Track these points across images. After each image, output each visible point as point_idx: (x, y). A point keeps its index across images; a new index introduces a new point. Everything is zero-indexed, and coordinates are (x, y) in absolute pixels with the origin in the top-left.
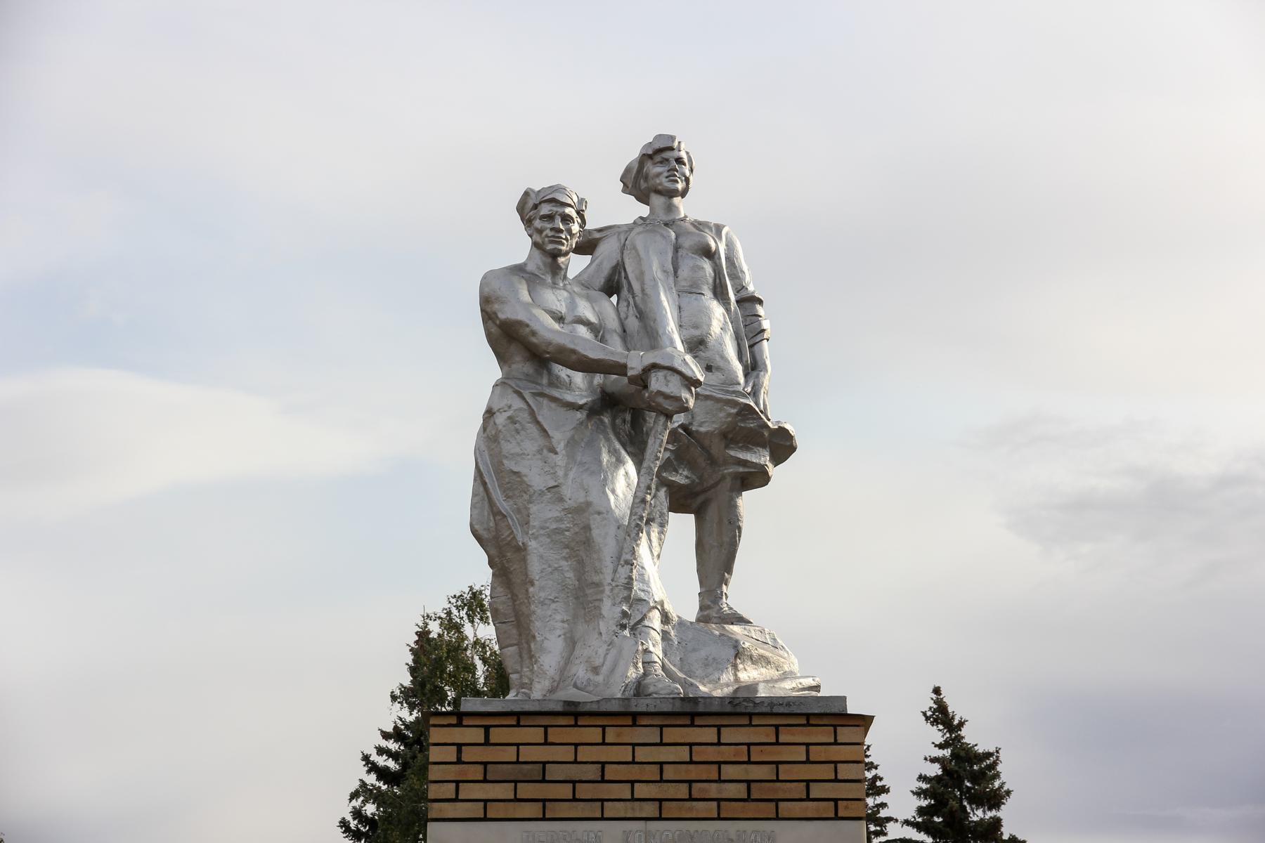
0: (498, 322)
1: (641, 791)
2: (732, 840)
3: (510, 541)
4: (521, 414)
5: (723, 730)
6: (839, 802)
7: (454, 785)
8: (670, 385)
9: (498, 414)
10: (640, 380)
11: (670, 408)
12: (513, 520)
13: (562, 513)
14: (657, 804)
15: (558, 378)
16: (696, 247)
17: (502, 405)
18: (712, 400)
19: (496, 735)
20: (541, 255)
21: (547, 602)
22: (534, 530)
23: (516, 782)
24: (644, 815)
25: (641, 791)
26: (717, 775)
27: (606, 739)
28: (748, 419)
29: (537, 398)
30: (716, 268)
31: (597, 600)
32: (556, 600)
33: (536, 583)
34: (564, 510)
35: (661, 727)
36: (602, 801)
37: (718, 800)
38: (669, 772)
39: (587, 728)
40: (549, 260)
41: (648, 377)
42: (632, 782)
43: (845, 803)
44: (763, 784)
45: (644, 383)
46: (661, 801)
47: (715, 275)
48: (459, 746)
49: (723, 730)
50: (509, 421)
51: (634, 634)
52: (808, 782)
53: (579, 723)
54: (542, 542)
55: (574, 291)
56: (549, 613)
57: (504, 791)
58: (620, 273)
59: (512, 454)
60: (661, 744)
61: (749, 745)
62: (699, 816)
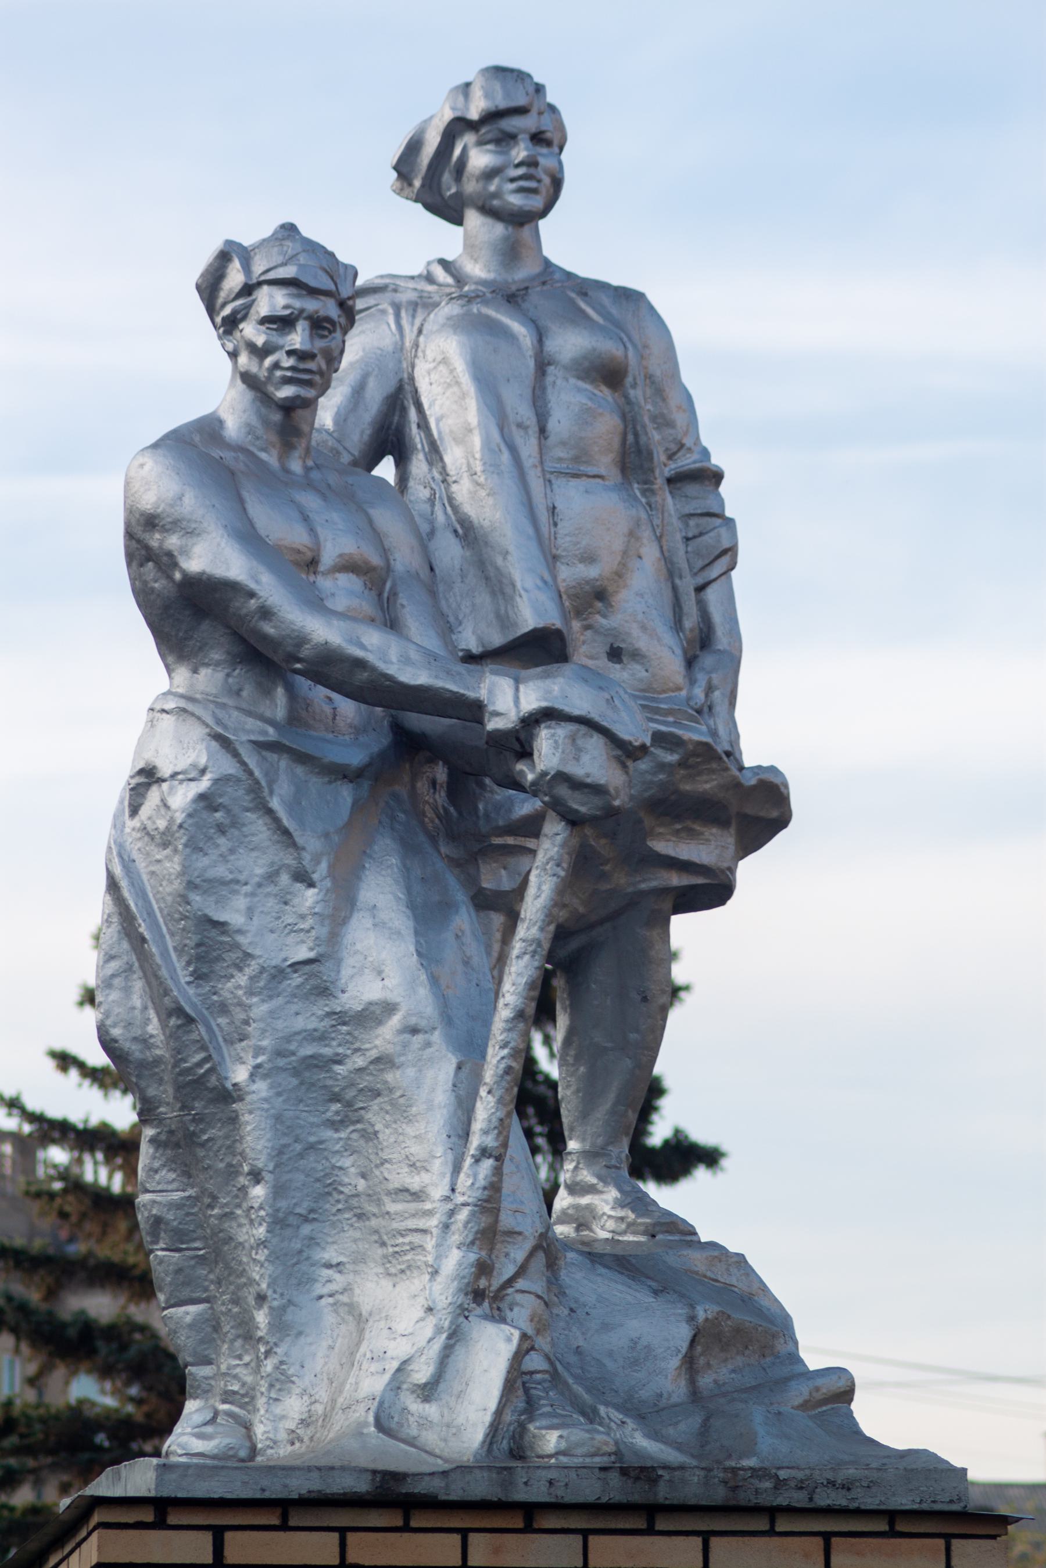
0: (178, 576)
3: (204, 1075)
4: (229, 790)
8: (585, 758)
10: (514, 740)
11: (583, 809)
13: (327, 1023)
15: (308, 705)
16: (586, 364)
20: (258, 404)
27: (469, 1558)
28: (700, 773)
29: (264, 753)
30: (627, 409)
31: (417, 1230)
32: (312, 1216)
33: (268, 1177)
34: (329, 1014)
35: (585, 1533)
39: (430, 1535)
40: (277, 417)
41: (531, 737)
45: (522, 746)
47: (626, 427)
49: (714, 1541)
50: (202, 804)
51: (499, 1309)
53: (413, 1524)
54: (280, 1085)
55: (329, 486)
56: (297, 1245)
58: (404, 410)
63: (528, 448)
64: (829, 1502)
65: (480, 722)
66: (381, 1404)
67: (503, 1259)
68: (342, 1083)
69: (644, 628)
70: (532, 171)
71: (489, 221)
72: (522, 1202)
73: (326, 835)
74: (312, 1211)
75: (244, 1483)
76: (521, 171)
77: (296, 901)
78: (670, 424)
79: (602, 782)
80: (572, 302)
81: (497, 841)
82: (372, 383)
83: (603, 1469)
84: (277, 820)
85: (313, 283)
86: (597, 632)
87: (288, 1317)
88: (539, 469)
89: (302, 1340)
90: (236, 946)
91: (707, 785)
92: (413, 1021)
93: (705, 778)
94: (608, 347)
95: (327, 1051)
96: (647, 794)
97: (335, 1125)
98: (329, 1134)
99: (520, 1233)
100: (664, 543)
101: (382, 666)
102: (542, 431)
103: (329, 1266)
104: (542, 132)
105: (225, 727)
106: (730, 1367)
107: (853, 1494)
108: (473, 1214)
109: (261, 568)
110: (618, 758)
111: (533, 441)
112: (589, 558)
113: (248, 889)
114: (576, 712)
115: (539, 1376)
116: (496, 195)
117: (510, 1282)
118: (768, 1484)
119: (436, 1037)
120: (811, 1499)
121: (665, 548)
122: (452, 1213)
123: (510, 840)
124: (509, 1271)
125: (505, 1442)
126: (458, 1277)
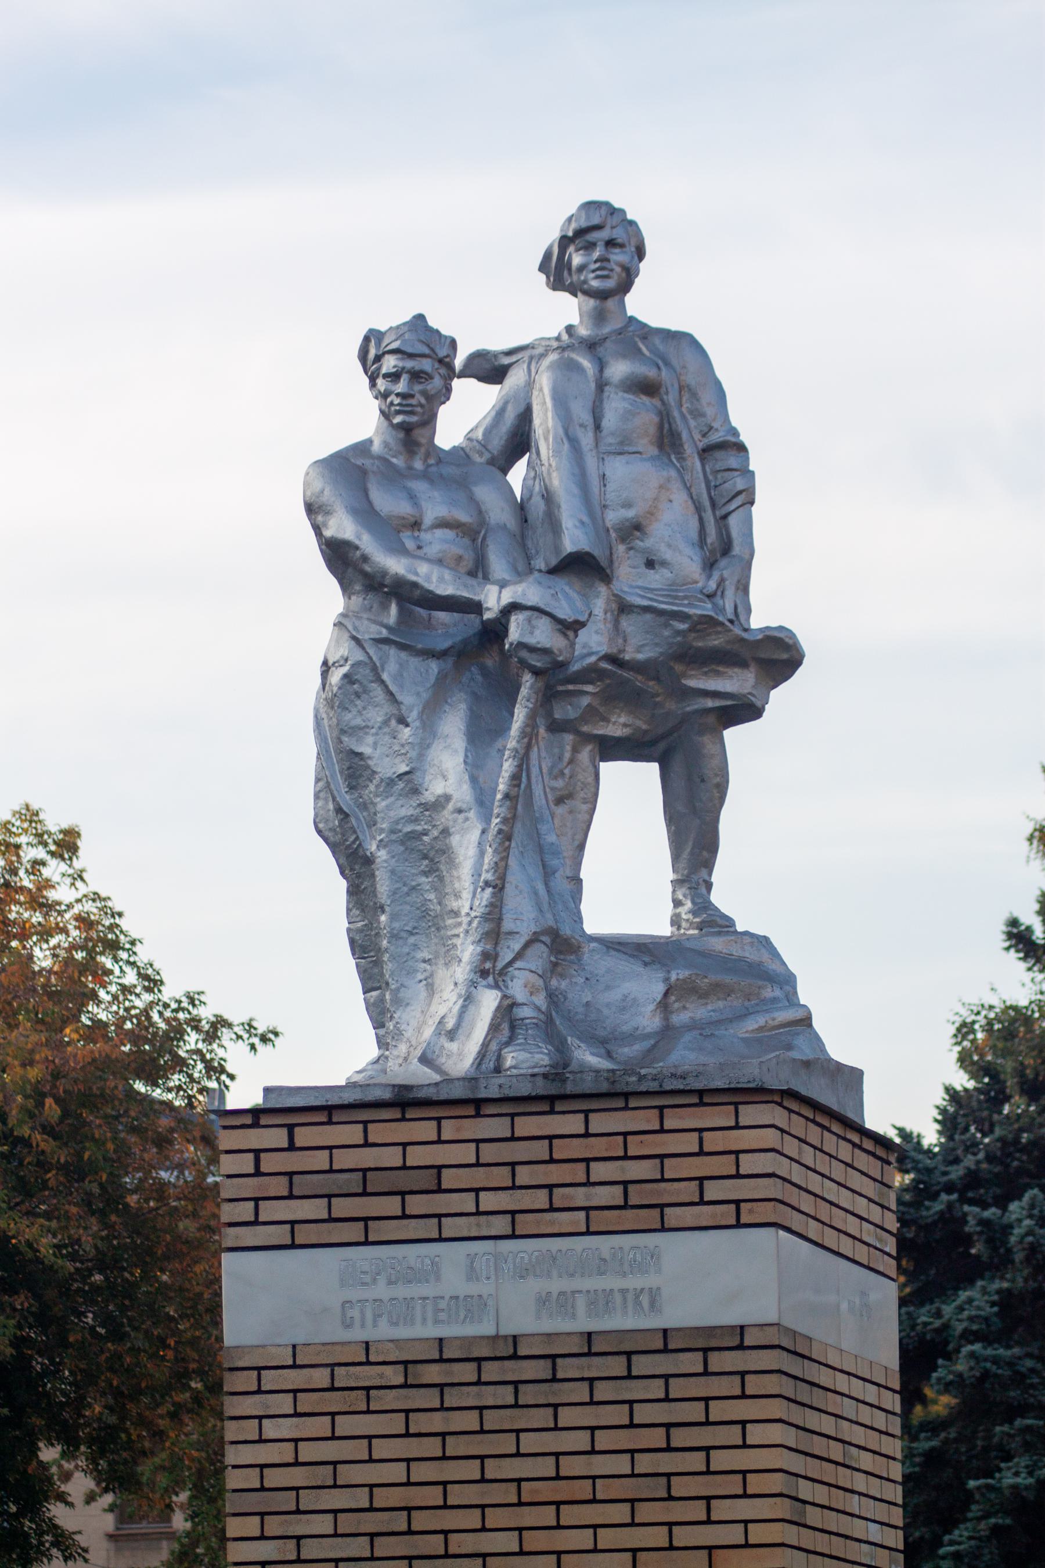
1: (488, 1201)
2: (605, 1260)
3: (356, 849)
5: (591, 1116)
6: (742, 1205)
7: (252, 1204)
8: (537, 632)
9: (333, 669)
11: (538, 664)
12: (357, 819)
13: (418, 810)
14: (509, 1217)
16: (629, 383)
17: (337, 657)
18: (652, 612)
19: (304, 1136)
21: (404, 935)
22: (383, 836)
23: (329, 1196)
24: (493, 1233)
25: (488, 1201)
26: (585, 1176)
28: (709, 634)
29: (380, 646)
33: (387, 909)
35: (513, 1116)
36: (439, 1216)
37: (587, 1209)
38: (524, 1175)
41: (508, 621)
42: (477, 1191)
43: (749, 1205)
44: (644, 1185)
46: (513, 1213)
48: (257, 1153)
49: (591, 1116)
52: (701, 1180)
53: (407, 1116)
56: (406, 950)
57: (315, 1209)
59: (352, 728)
60: (513, 1139)
61: (625, 1134)
62: (563, 1231)
63: (587, 440)
64: (673, 1087)
65: (481, 615)
66: (429, 1044)
67: (506, 950)
68: (428, 847)
69: (669, 546)
70: (605, 264)
71: (587, 298)
72: (522, 914)
73: (418, 694)
74: (415, 928)
75: (316, 1097)
76: (597, 265)
77: (399, 736)
78: (703, 415)
79: (548, 646)
80: (635, 344)
81: (560, 688)
82: (510, 408)
83: (533, 1075)
84: (386, 687)
85: (410, 350)
86: (637, 551)
87: (401, 995)
88: (594, 451)
89: (409, 1008)
90: (368, 767)
91: (716, 641)
92: (459, 805)
93: (713, 637)
94: (651, 373)
95: (419, 828)
96: (670, 651)
97: (425, 874)
98: (424, 879)
99: (517, 933)
100: (693, 490)
101: (426, 585)
102: (598, 427)
103: (424, 961)
104: (613, 240)
105: (358, 631)
106: (710, 1007)
107: (687, 1081)
108: (480, 923)
109: (363, 531)
110: (560, 630)
111: (591, 434)
112: (627, 505)
113: (373, 731)
114: (530, 604)
115: (528, 1021)
116: (585, 282)
117: (510, 963)
118: (634, 1079)
119: (472, 814)
120: (661, 1086)
121: (694, 494)
122: (470, 923)
123: (571, 687)
124: (509, 956)
125: (492, 1063)
126: (471, 963)
